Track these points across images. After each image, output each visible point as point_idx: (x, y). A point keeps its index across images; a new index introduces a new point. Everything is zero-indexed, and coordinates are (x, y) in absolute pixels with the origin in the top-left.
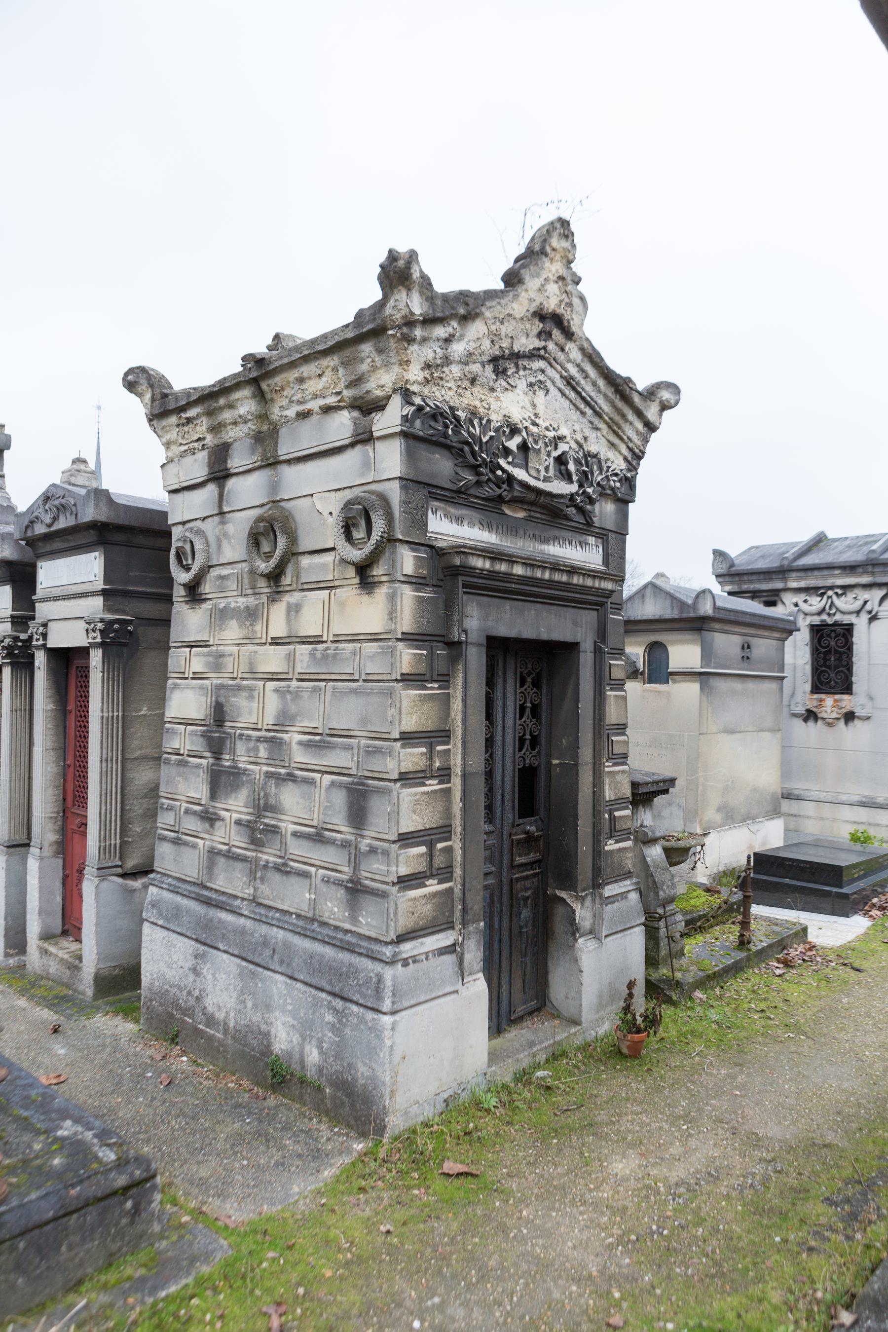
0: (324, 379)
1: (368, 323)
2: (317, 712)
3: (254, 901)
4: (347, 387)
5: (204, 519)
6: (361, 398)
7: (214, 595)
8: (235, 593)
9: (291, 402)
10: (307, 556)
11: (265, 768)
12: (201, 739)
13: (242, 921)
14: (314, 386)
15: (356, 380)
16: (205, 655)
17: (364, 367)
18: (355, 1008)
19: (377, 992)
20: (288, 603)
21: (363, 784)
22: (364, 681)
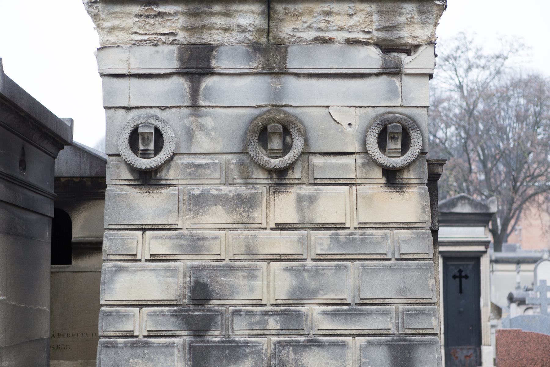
0: (356, 19)
2: (346, 285)
4: (378, 30)
6: (392, 40)
7: (181, 182)
8: (218, 182)
9: (310, 27)
10: (318, 156)
12: (173, 319)
14: (338, 20)
15: (390, 27)
17: (402, 19)
20: (298, 195)
22: (397, 259)
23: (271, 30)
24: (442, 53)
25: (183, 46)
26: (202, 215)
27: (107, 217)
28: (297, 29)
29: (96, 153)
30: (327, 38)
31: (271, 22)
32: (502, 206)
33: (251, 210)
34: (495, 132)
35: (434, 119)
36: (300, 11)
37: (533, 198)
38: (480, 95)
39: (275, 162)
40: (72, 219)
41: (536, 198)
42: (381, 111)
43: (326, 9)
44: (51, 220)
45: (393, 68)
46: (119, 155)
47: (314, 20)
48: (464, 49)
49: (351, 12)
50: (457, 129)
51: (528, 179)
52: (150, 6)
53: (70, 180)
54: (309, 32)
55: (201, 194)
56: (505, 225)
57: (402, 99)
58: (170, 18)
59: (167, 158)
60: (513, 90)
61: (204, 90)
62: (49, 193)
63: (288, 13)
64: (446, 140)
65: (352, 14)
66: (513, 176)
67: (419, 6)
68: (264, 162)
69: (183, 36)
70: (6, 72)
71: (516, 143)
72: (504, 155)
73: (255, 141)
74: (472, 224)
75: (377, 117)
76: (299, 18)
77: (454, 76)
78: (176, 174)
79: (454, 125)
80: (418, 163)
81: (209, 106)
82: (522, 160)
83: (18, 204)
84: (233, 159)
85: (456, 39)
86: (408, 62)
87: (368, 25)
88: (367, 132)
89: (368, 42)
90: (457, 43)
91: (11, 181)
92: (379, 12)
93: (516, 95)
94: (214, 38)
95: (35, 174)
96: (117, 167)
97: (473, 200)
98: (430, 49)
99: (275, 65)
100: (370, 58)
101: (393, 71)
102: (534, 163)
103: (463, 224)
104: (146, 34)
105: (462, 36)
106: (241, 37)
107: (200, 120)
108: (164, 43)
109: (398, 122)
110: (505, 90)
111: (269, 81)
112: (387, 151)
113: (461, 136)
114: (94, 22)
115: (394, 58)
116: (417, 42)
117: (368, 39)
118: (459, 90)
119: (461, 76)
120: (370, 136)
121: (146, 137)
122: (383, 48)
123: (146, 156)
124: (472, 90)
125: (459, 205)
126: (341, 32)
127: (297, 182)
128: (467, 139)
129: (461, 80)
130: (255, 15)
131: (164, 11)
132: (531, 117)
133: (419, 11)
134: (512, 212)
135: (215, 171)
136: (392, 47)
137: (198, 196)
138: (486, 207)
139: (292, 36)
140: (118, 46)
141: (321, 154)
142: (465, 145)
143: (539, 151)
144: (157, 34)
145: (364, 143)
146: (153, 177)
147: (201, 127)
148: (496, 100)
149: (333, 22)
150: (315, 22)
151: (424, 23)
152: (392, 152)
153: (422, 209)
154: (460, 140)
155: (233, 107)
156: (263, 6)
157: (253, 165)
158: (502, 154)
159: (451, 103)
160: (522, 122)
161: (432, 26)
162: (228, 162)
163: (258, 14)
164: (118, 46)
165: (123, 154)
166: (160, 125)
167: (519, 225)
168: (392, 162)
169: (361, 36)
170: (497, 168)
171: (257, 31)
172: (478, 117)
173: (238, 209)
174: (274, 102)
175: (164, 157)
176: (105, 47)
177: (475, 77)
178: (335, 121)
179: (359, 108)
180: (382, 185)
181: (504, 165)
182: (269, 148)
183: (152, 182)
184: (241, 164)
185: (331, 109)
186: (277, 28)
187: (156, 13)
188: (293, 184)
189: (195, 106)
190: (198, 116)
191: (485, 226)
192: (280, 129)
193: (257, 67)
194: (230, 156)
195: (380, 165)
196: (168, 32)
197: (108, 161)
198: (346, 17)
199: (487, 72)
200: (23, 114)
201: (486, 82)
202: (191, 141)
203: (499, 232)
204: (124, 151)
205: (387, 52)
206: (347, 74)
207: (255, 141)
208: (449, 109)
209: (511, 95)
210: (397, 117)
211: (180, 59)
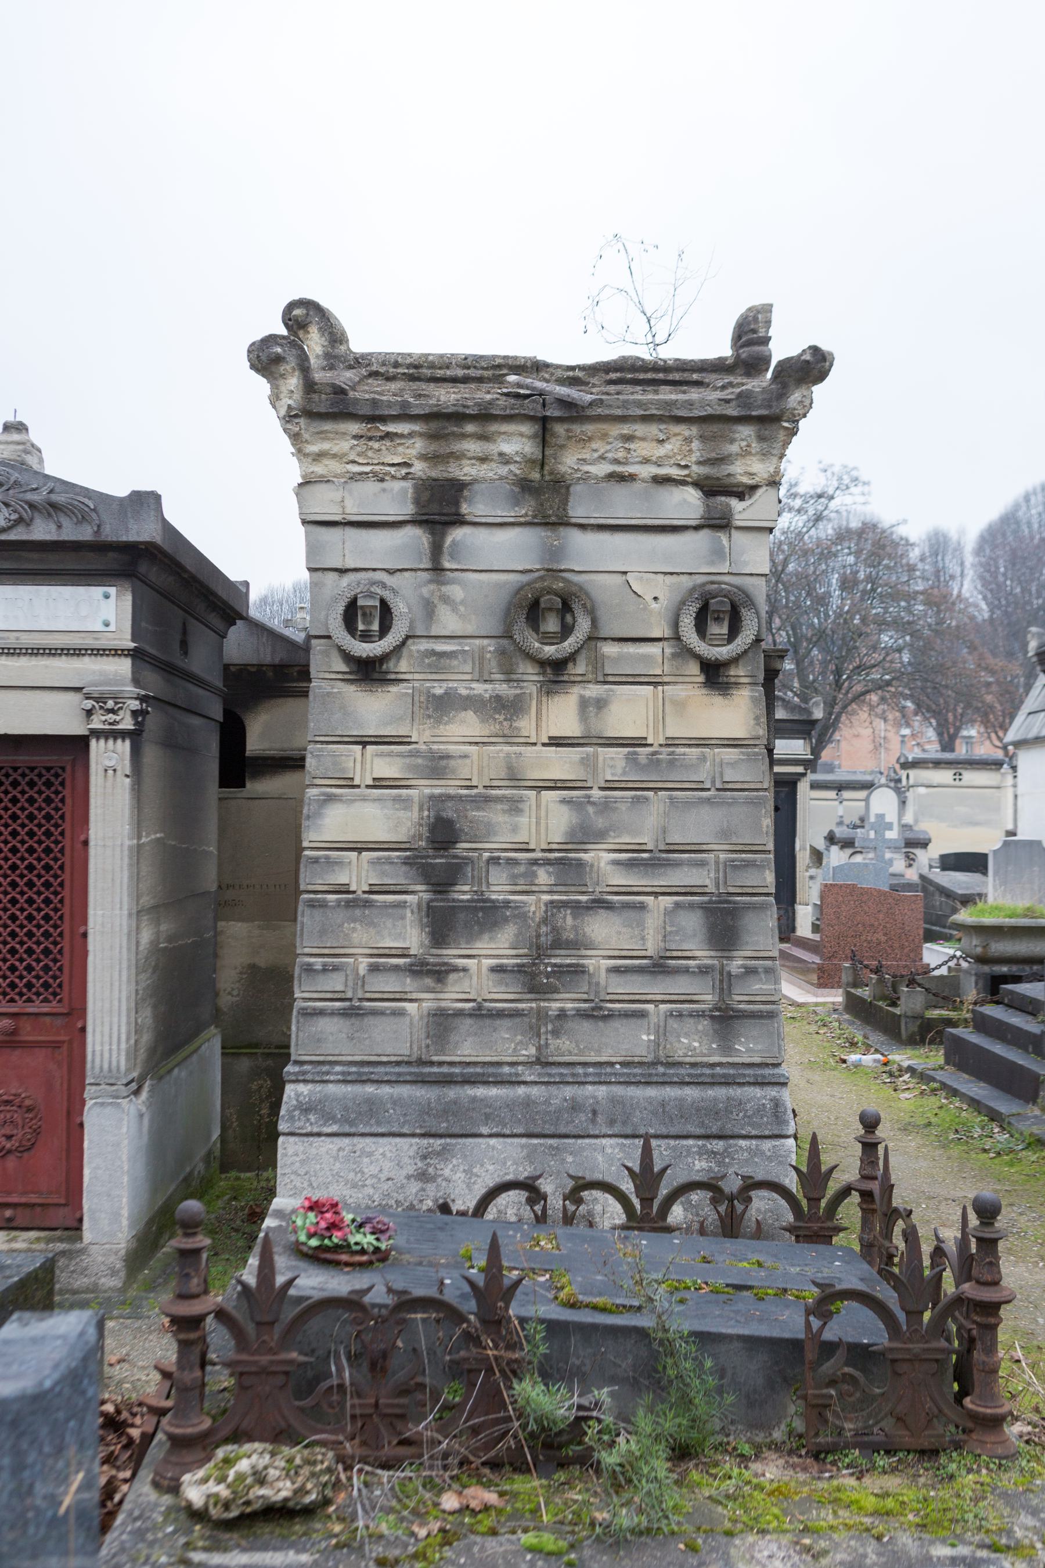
0: (668, 446)
1: (759, 407)
3: (541, 1062)
4: (699, 463)
5: (391, 572)
6: (718, 479)
7: (417, 676)
8: (468, 677)
9: (602, 458)
11: (546, 897)
12: (404, 868)
13: (521, 1090)
14: (642, 449)
16: (400, 755)
17: (734, 448)
18: (743, 1143)
19: (777, 1117)
20: (582, 697)
21: (729, 902)
22: (718, 790)
28: (584, 460)
39: (549, 651)
42: (700, 580)
46: (329, 637)
47: (608, 447)
49: (662, 437)
75: (693, 589)
80: (750, 654)
83: (179, 703)
84: (491, 646)
86: (741, 510)
94: (467, 471)
95: (200, 661)
96: (326, 653)
98: (772, 491)
100: (687, 504)
101: (719, 523)
106: (504, 470)
107: (443, 588)
108: (393, 477)
112: (708, 637)
127: (579, 679)
135: (465, 661)
137: (440, 697)
141: (614, 639)
145: (676, 625)
147: (446, 599)
151: (765, 455)
162: (482, 649)
163: (529, 437)
166: (387, 595)
177: (786, 525)
183: (376, 676)
184: (502, 653)
189: (437, 569)
193: (526, 515)
194: (486, 642)
198: (654, 444)
211: (417, 501)
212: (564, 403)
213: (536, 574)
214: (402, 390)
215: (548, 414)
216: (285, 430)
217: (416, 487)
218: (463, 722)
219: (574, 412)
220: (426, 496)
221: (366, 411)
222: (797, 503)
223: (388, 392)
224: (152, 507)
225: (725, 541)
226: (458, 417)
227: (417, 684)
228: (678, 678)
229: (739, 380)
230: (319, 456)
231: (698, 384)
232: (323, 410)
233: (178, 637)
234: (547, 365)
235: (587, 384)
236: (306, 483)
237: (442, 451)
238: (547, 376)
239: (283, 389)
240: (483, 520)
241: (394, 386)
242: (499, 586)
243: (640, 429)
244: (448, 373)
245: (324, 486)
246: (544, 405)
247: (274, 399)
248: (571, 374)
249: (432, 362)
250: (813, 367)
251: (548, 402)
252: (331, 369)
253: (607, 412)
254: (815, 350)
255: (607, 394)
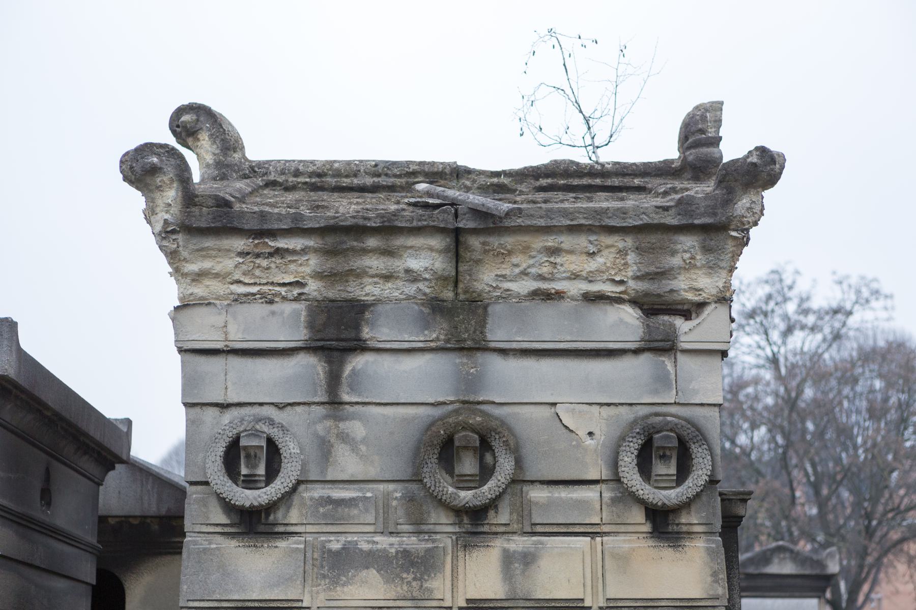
0: (600, 260)
1: (702, 215)
4: (636, 278)
5: (280, 406)
6: (659, 296)
7: (310, 529)
8: (370, 529)
9: (524, 273)
10: (539, 486)
14: (570, 263)
15: (657, 274)
17: (676, 261)
23: (460, 278)
24: (744, 305)
25: (316, 304)
26: (343, 585)
27: (185, 587)
28: (504, 276)
29: (168, 476)
30: (553, 291)
31: (460, 264)
32: (849, 561)
33: (426, 577)
34: (834, 436)
35: (731, 415)
36: (509, 247)
37: (899, 547)
38: (808, 374)
39: (466, 496)
40: (126, 587)
41: (905, 547)
42: (643, 411)
43: (550, 244)
44: (90, 588)
45: (661, 341)
46: (207, 483)
47: (531, 262)
48: (780, 299)
49: (592, 249)
50: (770, 431)
51: (890, 515)
52: (262, 238)
53: (124, 521)
54: (524, 282)
55: (343, 549)
56: (853, 591)
57: (677, 392)
58: (295, 258)
59: (287, 489)
60: (863, 366)
61: (350, 376)
62: (88, 545)
63: (489, 251)
64: (752, 450)
65: (594, 252)
66: (866, 509)
67: (704, 240)
68: (448, 496)
69: (315, 288)
70: (25, 345)
71: (870, 456)
72: (849, 474)
73: (433, 460)
74: (797, 594)
75: (635, 422)
76: (507, 259)
77: (763, 343)
78: (302, 515)
79: (765, 424)
80: (704, 498)
81: (357, 403)
82: (879, 484)
83: (37, 563)
84: (397, 491)
85: (767, 282)
86: (687, 331)
87: (620, 270)
88: (620, 446)
89: (620, 298)
90: (767, 289)
91: (23, 522)
92: (637, 249)
93: (867, 374)
94: (369, 290)
95: (67, 512)
96: (204, 503)
97: (798, 553)
98: (722, 310)
99: (466, 336)
100: (624, 324)
101: (662, 346)
102: (900, 487)
103: (783, 594)
104: (255, 284)
105: (776, 277)
106: (411, 289)
107: (341, 425)
108: (284, 298)
109: (671, 430)
110: (849, 366)
111: (458, 361)
112: (654, 478)
113: (776, 443)
114: (169, 263)
115: (663, 325)
116: (700, 297)
117: (620, 293)
118: (773, 365)
119: (775, 343)
120: (624, 454)
121: (252, 454)
122: (645, 307)
123: (251, 486)
124: (794, 366)
125: (776, 560)
126: (575, 282)
127: (502, 529)
128: (786, 448)
129: (775, 349)
130: (434, 254)
131: (286, 246)
132: (893, 411)
133: (704, 247)
134: (866, 570)
135: (367, 510)
136: (659, 307)
137: (337, 553)
138: (821, 564)
139: (494, 288)
140: (209, 304)
141: (542, 482)
142: (784, 458)
143: (907, 467)
144: (272, 283)
145: (615, 465)
146: (263, 521)
147: (344, 438)
148: (833, 383)
149: (562, 265)
150: (532, 266)
151: (712, 268)
152: (662, 480)
153: (712, 575)
154: (775, 450)
155: (398, 404)
156: (448, 240)
157: (429, 501)
158: (847, 472)
159: (760, 387)
160: (879, 420)
161: (725, 271)
162: (387, 496)
163: (440, 252)
164: (209, 304)
165: (214, 482)
166: (275, 433)
167: (877, 593)
168: (662, 497)
169: (608, 289)
170: (838, 497)
171: (437, 279)
172: (804, 410)
173: (405, 575)
174: (464, 396)
175: (281, 487)
176: (188, 305)
177: (799, 345)
178: (566, 427)
179: (606, 407)
180: (645, 535)
181: (851, 492)
182: (457, 472)
183: (261, 528)
184: (410, 499)
185: (560, 409)
186: (470, 275)
187: (272, 250)
188: (496, 533)
189: (334, 403)
190: (338, 419)
191: (819, 597)
192: (475, 441)
193: (437, 339)
194: (391, 487)
195: (641, 502)
196: (292, 280)
197: (188, 493)
198: (584, 257)
199: (819, 337)
200: (49, 414)
201: (816, 352)
202: (327, 460)
203: (844, 605)
204: (216, 477)
205: (652, 314)
206: (586, 351)
207: (433, 460)
208: (756, 398)
209: (860, 374)
210: (669, 422)
211: (311, 325)
212: (478, 213)
213: (450, 408)
214: (298, 201)
215: (461, 225)
216: (161, 247)
217: (310, 309)
218: (364, 582)
219: (490, 223)
220: (321, 319)
221: (253, 225)
222: (811, 320)
223: (279, 204)
224: (6, 336)
225: (670, 367)
226: (358, 230)
227: (310, 538)
228: (619, 527)
229: (686, 184)
230: (199, 277)
231: (640, 189)
232: (204, 225)
233: (38, 485)
234: (468, 172)
235: (513, 191)
236: (184, 307)
237: (340, 268)
238: (468, 183)
239: (160, 202)
240: (388, 346)
241: (290, 197)
242: (406, 420)
243: (566, 241)
244: (356, 181)
245: (204, 310)
246: (456, 215)
247: (149, 214)
248: (495, 180)
249: (338, 170)
250: (763, 169)
251: (460, 212)
252: (222, 179)
253: (528, 223)
254: (762, 151)
255: (534, 202)
